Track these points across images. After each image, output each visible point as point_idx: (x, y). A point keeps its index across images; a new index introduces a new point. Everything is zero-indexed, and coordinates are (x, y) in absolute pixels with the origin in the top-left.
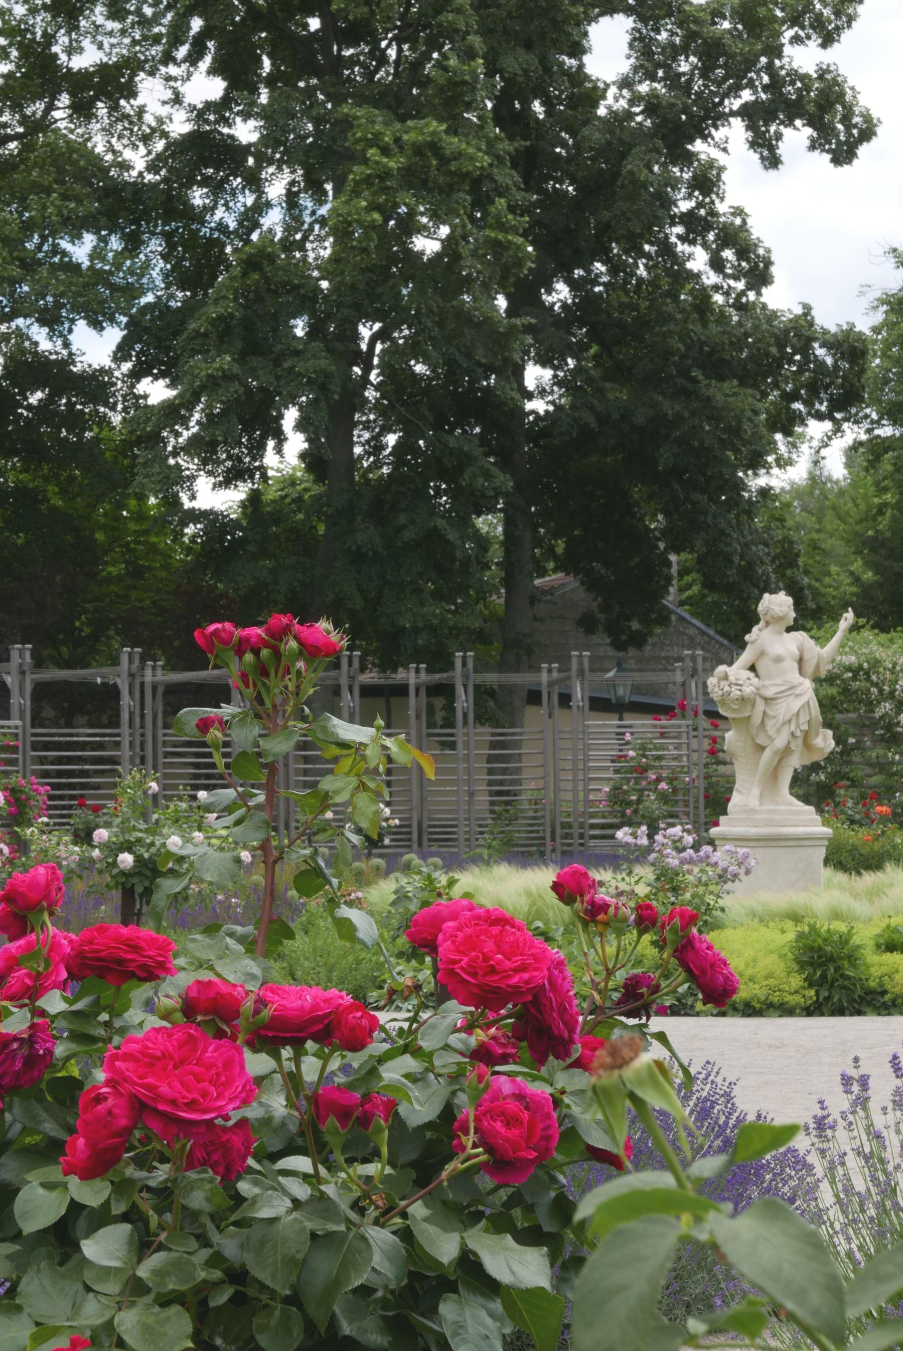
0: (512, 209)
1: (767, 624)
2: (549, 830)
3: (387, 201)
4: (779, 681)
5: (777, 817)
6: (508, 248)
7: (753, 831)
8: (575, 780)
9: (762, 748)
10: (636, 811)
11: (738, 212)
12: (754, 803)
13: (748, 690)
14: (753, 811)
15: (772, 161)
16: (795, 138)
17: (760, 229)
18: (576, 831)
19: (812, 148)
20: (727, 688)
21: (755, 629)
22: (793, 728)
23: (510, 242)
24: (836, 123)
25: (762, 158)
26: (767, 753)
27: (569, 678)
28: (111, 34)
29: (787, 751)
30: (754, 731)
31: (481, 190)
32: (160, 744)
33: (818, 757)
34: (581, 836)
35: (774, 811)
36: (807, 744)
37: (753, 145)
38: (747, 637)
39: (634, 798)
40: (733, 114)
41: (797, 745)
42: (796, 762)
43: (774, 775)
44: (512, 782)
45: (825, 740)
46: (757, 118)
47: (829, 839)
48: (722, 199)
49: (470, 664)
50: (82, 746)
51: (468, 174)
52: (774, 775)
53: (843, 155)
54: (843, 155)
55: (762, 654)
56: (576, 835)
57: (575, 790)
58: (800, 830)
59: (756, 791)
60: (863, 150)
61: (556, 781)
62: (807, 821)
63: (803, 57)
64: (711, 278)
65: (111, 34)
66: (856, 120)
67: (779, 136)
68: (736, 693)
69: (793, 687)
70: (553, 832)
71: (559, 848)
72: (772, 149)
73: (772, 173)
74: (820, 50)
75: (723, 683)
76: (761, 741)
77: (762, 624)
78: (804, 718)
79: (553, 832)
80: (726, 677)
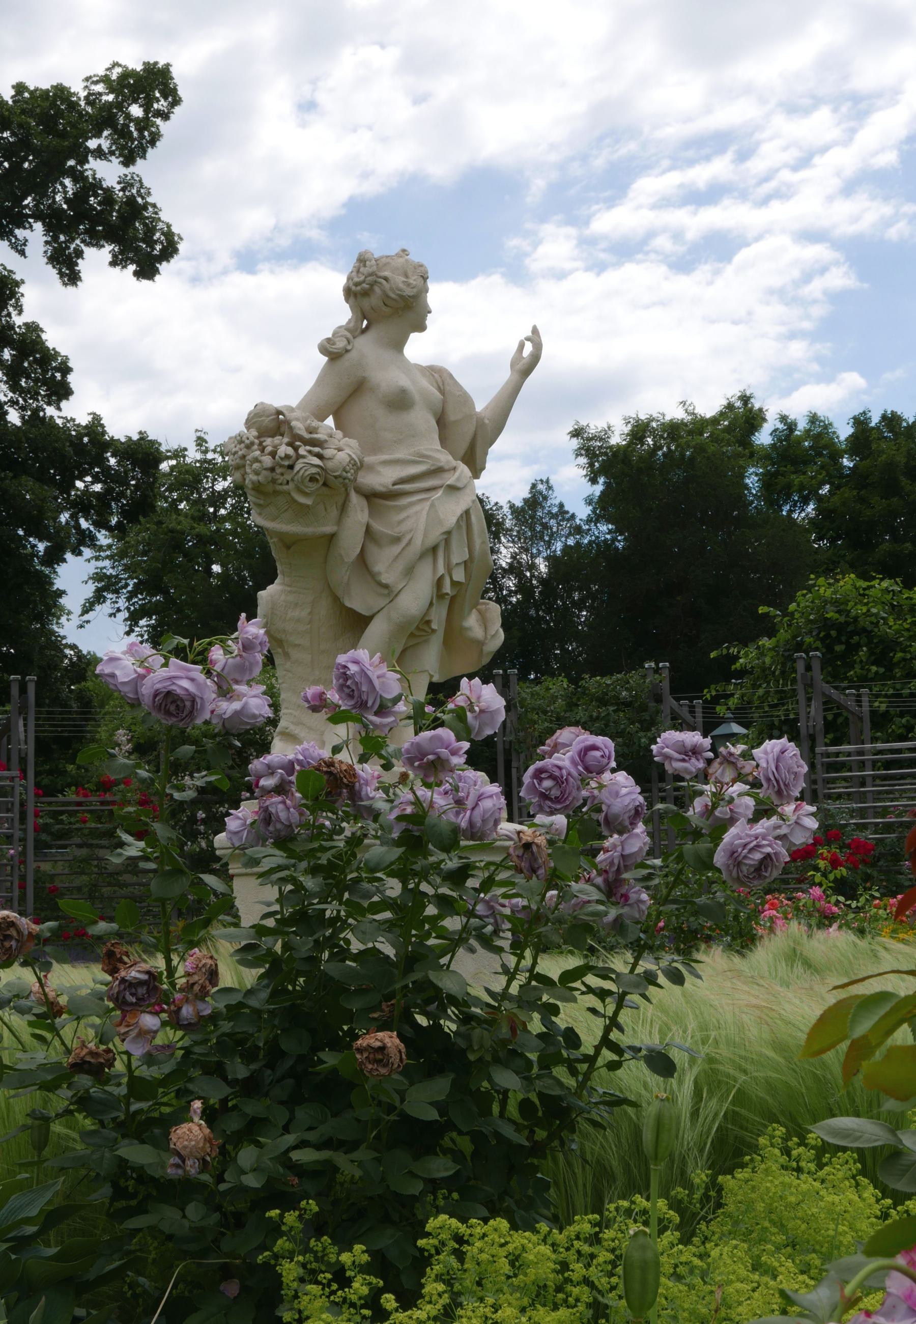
11: (33, 328)
16: (95, 260)
17: (52, 338)
22: (441, 570)
24: (142, 244)
25: (61, 275)
45: (484, 622)
46: (55, 223)
48: (20, 312)
50: (70, 732)
54: (147, 271)
63: (108, 172)
67: (79, 254)
68: (308, 462)
73: (70, 289)
76: (358, 602)
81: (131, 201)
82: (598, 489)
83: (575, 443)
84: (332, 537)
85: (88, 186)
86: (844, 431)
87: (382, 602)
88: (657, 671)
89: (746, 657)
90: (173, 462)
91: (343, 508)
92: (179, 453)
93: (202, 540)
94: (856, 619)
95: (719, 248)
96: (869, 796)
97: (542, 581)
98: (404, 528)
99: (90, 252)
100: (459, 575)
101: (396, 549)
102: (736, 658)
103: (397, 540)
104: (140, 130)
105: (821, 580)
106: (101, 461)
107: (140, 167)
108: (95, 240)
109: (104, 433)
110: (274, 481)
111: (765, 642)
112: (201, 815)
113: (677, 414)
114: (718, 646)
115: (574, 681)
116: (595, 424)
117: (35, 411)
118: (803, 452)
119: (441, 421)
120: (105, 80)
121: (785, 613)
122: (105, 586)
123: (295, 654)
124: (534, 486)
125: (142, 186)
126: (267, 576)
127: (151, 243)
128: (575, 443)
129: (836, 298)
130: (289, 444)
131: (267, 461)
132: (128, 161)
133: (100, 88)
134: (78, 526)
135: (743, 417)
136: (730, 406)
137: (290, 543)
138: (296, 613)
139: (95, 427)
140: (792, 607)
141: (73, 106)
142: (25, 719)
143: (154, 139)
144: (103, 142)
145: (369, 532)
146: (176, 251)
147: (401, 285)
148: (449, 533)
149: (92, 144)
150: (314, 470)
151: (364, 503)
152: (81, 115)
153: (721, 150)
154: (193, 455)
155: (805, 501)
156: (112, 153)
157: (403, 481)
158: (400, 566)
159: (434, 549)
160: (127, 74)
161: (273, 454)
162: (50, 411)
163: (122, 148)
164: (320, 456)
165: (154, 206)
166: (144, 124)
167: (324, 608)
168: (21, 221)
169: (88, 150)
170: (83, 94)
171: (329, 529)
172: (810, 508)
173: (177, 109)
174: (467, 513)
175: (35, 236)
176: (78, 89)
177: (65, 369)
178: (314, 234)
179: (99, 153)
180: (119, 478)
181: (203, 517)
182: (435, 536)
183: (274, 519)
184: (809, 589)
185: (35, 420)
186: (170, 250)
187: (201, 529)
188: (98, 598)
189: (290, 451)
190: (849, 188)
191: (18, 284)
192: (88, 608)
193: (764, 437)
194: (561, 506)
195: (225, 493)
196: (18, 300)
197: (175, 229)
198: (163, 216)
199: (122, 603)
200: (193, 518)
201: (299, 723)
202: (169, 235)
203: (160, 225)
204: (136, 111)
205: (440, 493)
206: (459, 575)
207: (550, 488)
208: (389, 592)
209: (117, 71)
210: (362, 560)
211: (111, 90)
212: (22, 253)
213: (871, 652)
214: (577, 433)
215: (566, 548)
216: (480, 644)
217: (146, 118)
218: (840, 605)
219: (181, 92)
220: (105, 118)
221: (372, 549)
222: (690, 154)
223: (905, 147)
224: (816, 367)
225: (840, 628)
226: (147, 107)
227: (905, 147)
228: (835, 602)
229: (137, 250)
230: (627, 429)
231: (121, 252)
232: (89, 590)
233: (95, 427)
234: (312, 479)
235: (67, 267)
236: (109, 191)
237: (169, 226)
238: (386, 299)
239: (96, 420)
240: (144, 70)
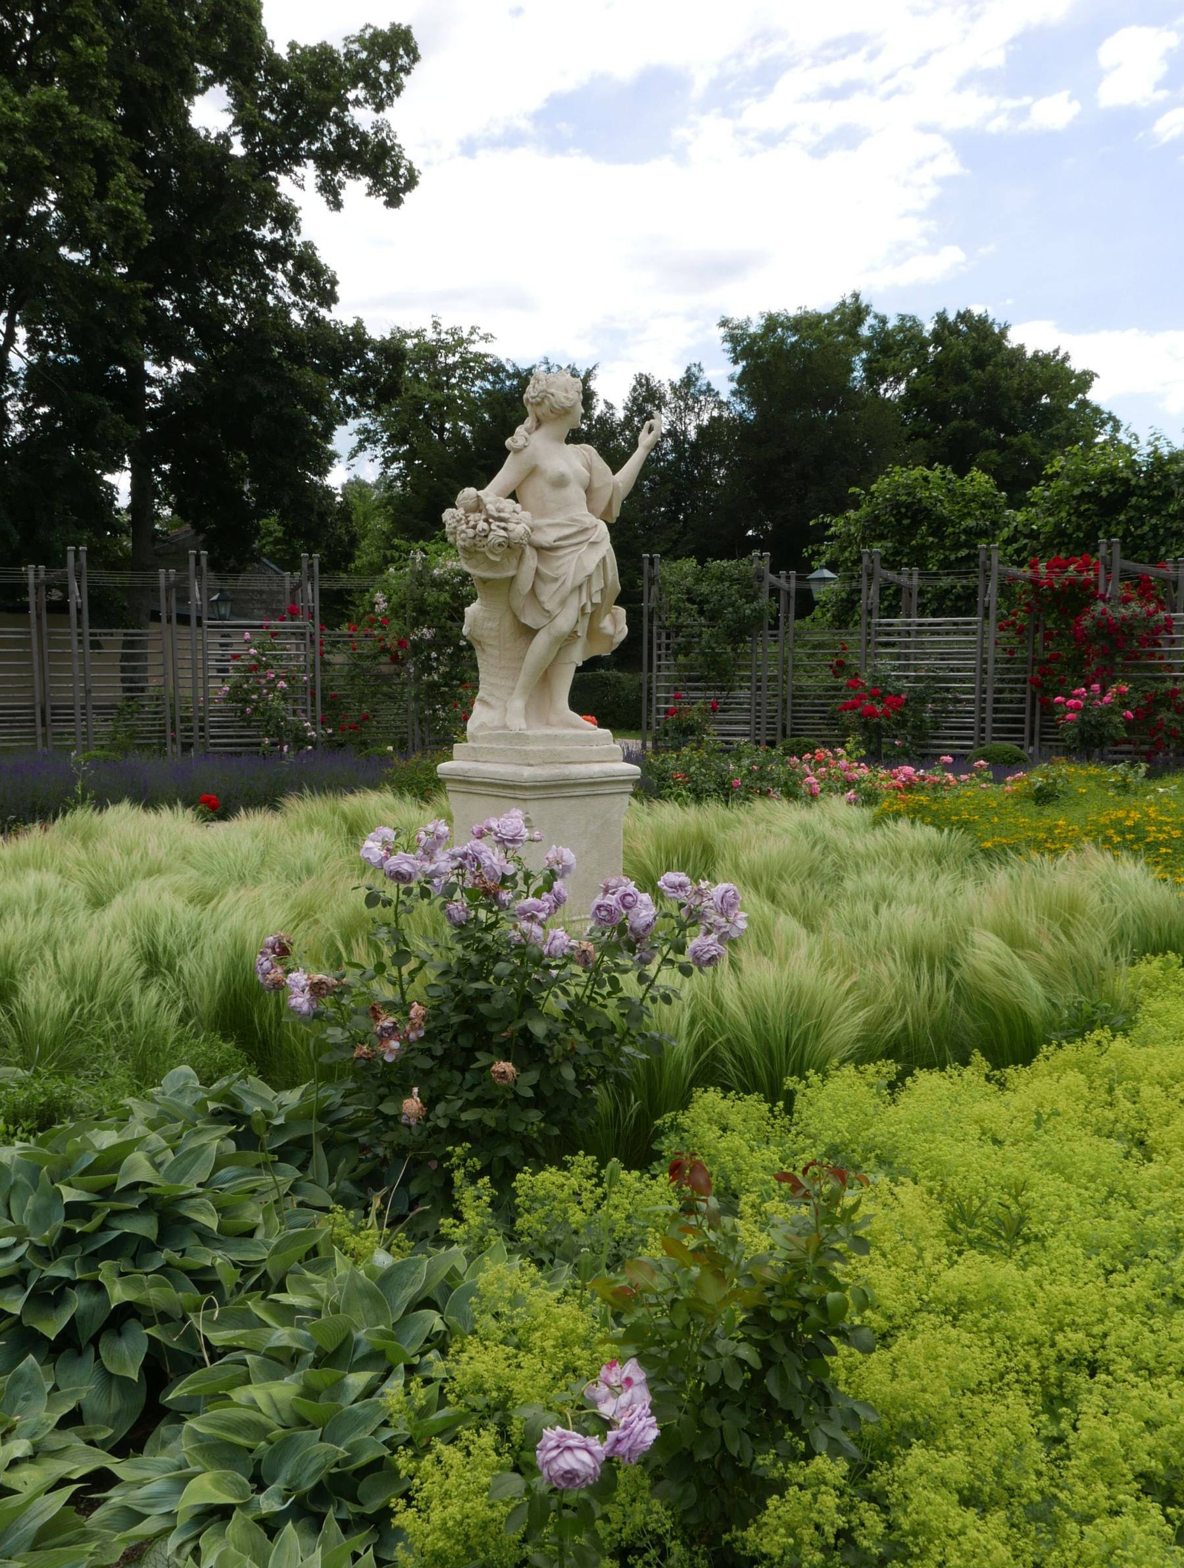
0: (130, 184)
1: (539, 423)
2: (169, 721)
3: (15, 154)
5: (561, 748)
6: (127, 218)
7: (527, 773)
8: (195, 678)
9: (530, 633)
10: (255, 709)
11: (308, 245)
12: (518, 723)
13: (518, 530)
14: (520, 737)
15: (337, 205)
16: (355, 188)
17: (324, 256)
18: (196, 724)
20: (482, 525)
21: (520, 430)
22: (584, 600)
23: (129, 212)
24: (383, 167)
25: (328, 202)
26: (541, 642)
27: (187, 578)
29: (572, 637)
30: (518, 602)
31: (102, 160)
33: (604, 650)
34: (202, 729)
35: (556, 738)
36: (593, 632)
38: (508, 442)
39: (254, 697)
43: (545, 679)
44: (141, 680)
45: (615, 622)
46: (326, 162)
48: (299, 233)
49: (83, 558)
50: (945, 738)
51: (91, 142)
52: (545, 679)
53: (394, 200)
54: (394, 200)
55: (533, 472)
56: (196, 729)
57: (194, 687)
58: (595, 769)
59: (518, 704)
60: (407, 197)
61: (175, 677)
62: (604, 753)
63: (362, 117)
64: (288, 297)
66: (402, 171)
67: (342, 185)
68: (497, 534)
69: (584, 531)
70: (173, 723)
71: (179, 740)
72: (336, 194)
73: (335, 213)
75: (472, 517)
76: (529, 620)
77: (529, 422)
78: (597, 585)
79: (173, 723)
80: (479, 506)
81: (382, 143)
82: (738, 369)
83: (722, 331)
84: (513, 578)
85: (349, 131)
86: (929, 327)
87: (545, 621)
88: (761, 558)
89: (838, 525)
90: (416, 341)
91: (521, 559)
92: (418, 335)
93: (437, 405)
94: (920, 500)
95: (848, 137)
97: (691, 444)
98: (560, 572)
99: (350, 183)
100: (597, 599)
101: (556, 586)
102: (829, 526)
103: (556, 580)
104: (388, 82)
105: (897, 468)
106: (362, 355)
107: (388, 114)
111: (851, 514)
112: (434, 655)
113: (656, 804)
114: (816, 516)
115: (701, 562)
116: (738, 315)
117: (312, 313)
118: (895, 346)
119: (588, 490)
120: (360, 39)
121: (868, 492)
122: (367, 438)
123: (489, 650)
124: (689, 369)
126: (470, 599)
127: (396, 176)
128: (722, 331)
129: (944, 182)
130: (486, 520)
131: (471, 532)
132: (379, 108)
133: (355, 47)
134: (345, 402)
135: (854, 313)
136: (843, 304)
137: (484, 581)
138: (490, 625)
139: (358, 329)
140: (874, 487)
141: (334, 61)
143: (399, 89)
145: (537, 572)
146: (416, 183)
148: (590, 577)
151: (535, 553)
152: (341, 69)
153: (855, 49)
154: (430, 335)
155: (898, 381)
156: (366, 101)
157: (560, 539)
158: (557, 598)
159: (580, 587)
160: (377, 34)
161: (474, 527)
162: (323, 312)
163: (374, 97)
164: (505, 529)
166: (391, 77)
167: (508, 621)
168: (298, 161)
169: (348, 101)
170: (343, 51)
171: (511, 573)
172: (903, 386)
173: (417, 66)
174: (604, 559)
175: (309, 172)
176: (339, 47)
177: (334, 283)
178: (524, 125)
179: (357, 102)
180: (376, 370)
181: (438, 386)
182: (581, 578)
183: (475, 567)
184: (888, 474)
185: (312, 319)
186: (412, 182)
187: (437, 396)
188: (361, 447)
189: (485, 526)
190: (961, 85)
192: (353, 455)
193: (865, 331)
194: (709, 384)
195: (455, 366)
197: (415, 166)
198: (406, 154)
199: (379, 451)
200: (431, 387)
201: (491, 695)
202: (411, 170)
203: (404, 163)
204: (385, 66)
205: (585, 547)
206: (597, 599)
207: (701, 370)
208: (550, 616)
209: (370, 31)
210: (533, 592)
211: (365, 48)
212: (302, 187)
213: (930, 527)
214: (724, 324)
215: (712, 418)
216: (612, 637)
217: (392, 72)
218: (910, 490)
219: (420, 51)
220: (362, 74)
221: (539, 584)
222: (828, 53)
223: (1011, 48)
224: (924, 242)
225: (908, 506)
227: (1011, 48)
228: (906, 486)
229: (386, 184)
230: (762, 322)
231: (375, 185)
232: (355, 439)
233: (358, 329)
234: (500, 545)
235: (331, 193)
236: (364, 135)
238: (552, 410)
239: (359, 323)
240: (391, 30)
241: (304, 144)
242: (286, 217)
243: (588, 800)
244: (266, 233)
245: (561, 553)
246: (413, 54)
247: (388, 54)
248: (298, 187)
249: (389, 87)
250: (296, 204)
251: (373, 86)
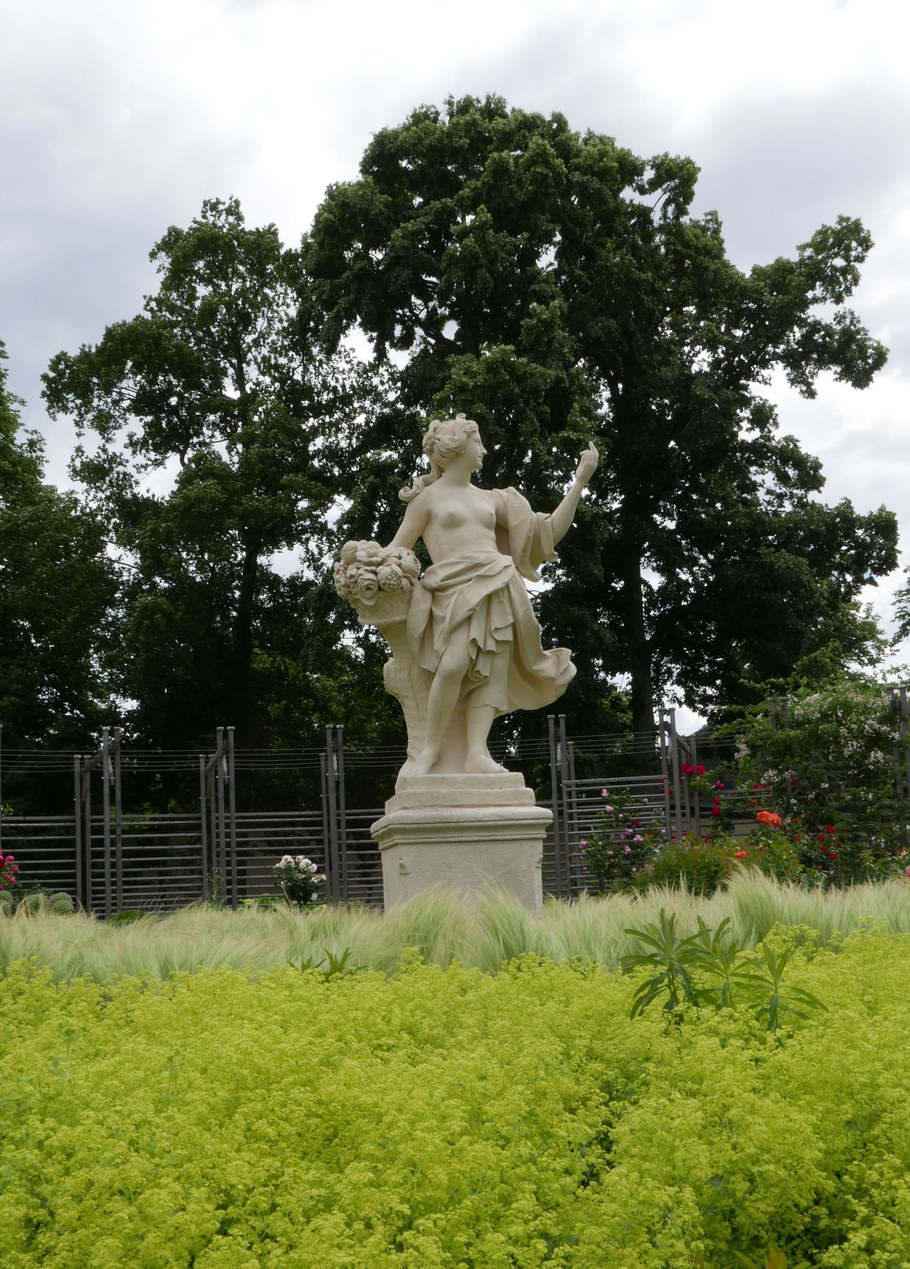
4: (453, 559)
5: (445, 790)
9: (430, 675)
16: (826, 380)
19: (699, 169)
24: (855, 358)
26: (437, 680)
28: (343, 372)
32: (88, 855)
37: (793, 382)
40: (776, 357)
41: (496, 670)
42: (495, 700)
45: (558, 663)
46: (793, 360)
47: (549, 828)
53: (861, 379)
54: (861, 379)
55: (428, 518)
62: (513, 798)
63: (822, 312)
65: (343, 372)
69: (479, 566)
72: (808, 385)
74: (834, 305)
78: (500, 618)
91: (409, 602)
96: (576, 837)
107: (849, 302)
108: (822, 363)
109: (852, 513)
110: (350, 592)
117: (800, 499)
125: (853, 318)
127: (864, 358)
132: (838, 299)
142: (227, 758)
144: (819, 291)
147: (447, 442)
149: (810, 295)
150: (367, 583)
164: (375, 573)
165: (863, 329)
171: (398, 618)
175: (778, 372)
179: (815, 300)
182: (462, 614)
185: (802, 504)
186: (880, 358)
191: (772, 408)
196: (774, 420)
226: (847, 258)
234: (368, 588)
237: (878, 343)
241: (770, 349)
242: (763, 416)
243: (482, 846)
244: (747, 434)
245: (450, 591)
246: (866, 243)
247: (839, 249)
248: (772, 386)
249: (845, 279)
250: (772, 402)
251: (830, 282)
